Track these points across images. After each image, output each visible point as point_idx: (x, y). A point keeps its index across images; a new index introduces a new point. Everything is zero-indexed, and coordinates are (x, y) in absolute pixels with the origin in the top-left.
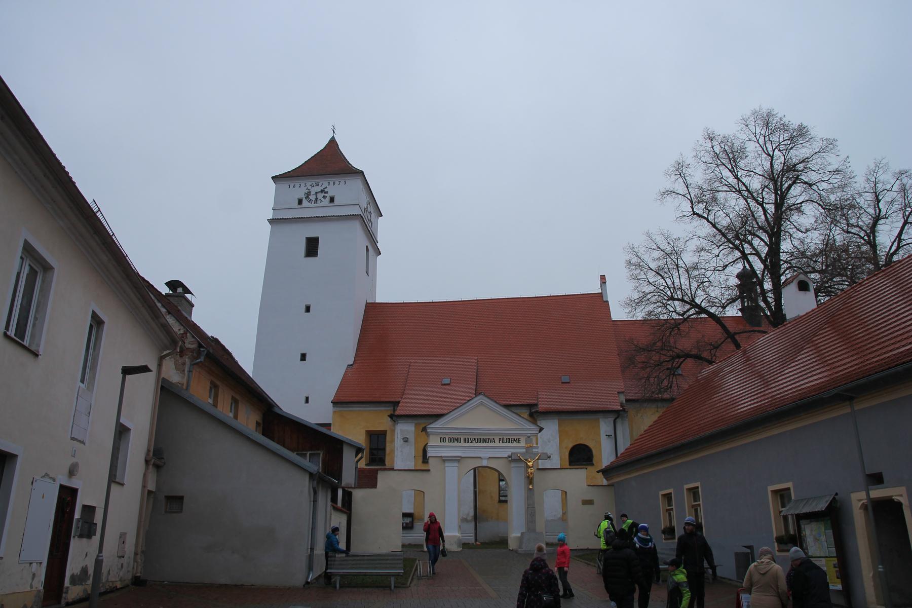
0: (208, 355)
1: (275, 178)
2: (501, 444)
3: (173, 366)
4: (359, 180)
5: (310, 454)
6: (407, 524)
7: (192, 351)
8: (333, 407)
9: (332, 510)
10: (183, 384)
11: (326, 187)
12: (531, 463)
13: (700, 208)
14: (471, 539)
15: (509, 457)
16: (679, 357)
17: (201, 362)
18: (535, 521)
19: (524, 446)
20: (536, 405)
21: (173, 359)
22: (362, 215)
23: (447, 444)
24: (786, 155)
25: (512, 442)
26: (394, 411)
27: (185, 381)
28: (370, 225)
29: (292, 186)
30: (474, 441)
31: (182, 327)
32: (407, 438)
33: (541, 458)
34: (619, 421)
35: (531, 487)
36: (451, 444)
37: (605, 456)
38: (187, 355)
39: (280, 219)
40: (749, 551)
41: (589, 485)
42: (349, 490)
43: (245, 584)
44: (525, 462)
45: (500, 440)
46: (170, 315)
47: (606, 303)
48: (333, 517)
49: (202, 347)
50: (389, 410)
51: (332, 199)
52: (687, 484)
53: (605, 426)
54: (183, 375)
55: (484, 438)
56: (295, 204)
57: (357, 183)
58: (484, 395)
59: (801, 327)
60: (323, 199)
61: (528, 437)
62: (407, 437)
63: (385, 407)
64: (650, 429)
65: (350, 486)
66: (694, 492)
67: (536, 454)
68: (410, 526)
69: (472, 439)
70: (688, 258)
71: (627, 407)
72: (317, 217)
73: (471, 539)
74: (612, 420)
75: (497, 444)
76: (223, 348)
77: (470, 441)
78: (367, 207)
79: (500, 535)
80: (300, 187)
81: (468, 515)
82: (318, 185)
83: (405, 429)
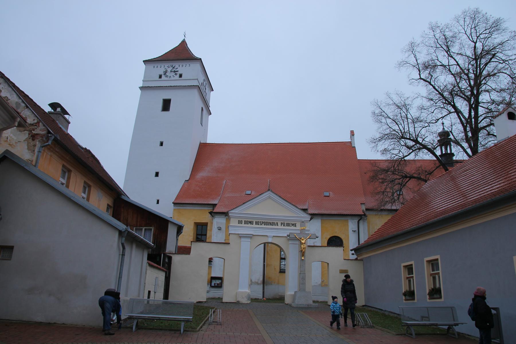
0: (56, 140)
1: (144, 61)
2: (283, 227)
3: (26, 147)
4: (199, 64)
5: (145, 229)
6: (218, 284)
7: (42, 136)
9: (148, 266)
10: (32, 161)
11: (177, 68)
12: (304, 241)
13: (425, 75)
14: (260, 296)
15: (288, 236)
16: (406, 177)
17: (49, 145)
18: (305, 283)
19: (299, 229)
21: (26, 142)
22: (199, 86)
23: (243, 225)
24: (484, 43)
25: (291, 226)
26: (213, 210)
27: (34, 159)
28: (205, 94)
29: (156, 66)
30: (263, 224)
31: (36, 118)
32: (221, 228)
33: (310, 238)
34: (361, 222)
35: (303, 258)
36: (246, 225)
37: (352, 242)
38: (37, 139)
39: (147, 87)
41: (345, 259)
42: (170, 255)
43: (57, 323)
44: (299, 240)
45: (282, 224)
46: (28, 109)
47: (353, 148)
49: (51, 133)
50: (210, 209)
51: (181, 76)
52: (427, 257)
53: (352, 225)
54: (33, 154)
55: (270, 223)
56: (157, 78)
57: (196, 66)
58: (272, 191)
59: (462, 181)
60: (175, 76)
62: (221, 227)
63: (208, 207)
64: (389, 222)
65: (172, 253)
66: (434, 264)
67: (308, 234)
68: (220, 286)
69: (261, 222)
70: (414, 113)
71: (367, 213)
73: (260, 296)
74: (356, 221)
75: (279, 227)
76: (93, 156)
78: (203, 83)
79: (279, 294)
80: (161, 67)
81: (259, 280)
83: (219, 221)
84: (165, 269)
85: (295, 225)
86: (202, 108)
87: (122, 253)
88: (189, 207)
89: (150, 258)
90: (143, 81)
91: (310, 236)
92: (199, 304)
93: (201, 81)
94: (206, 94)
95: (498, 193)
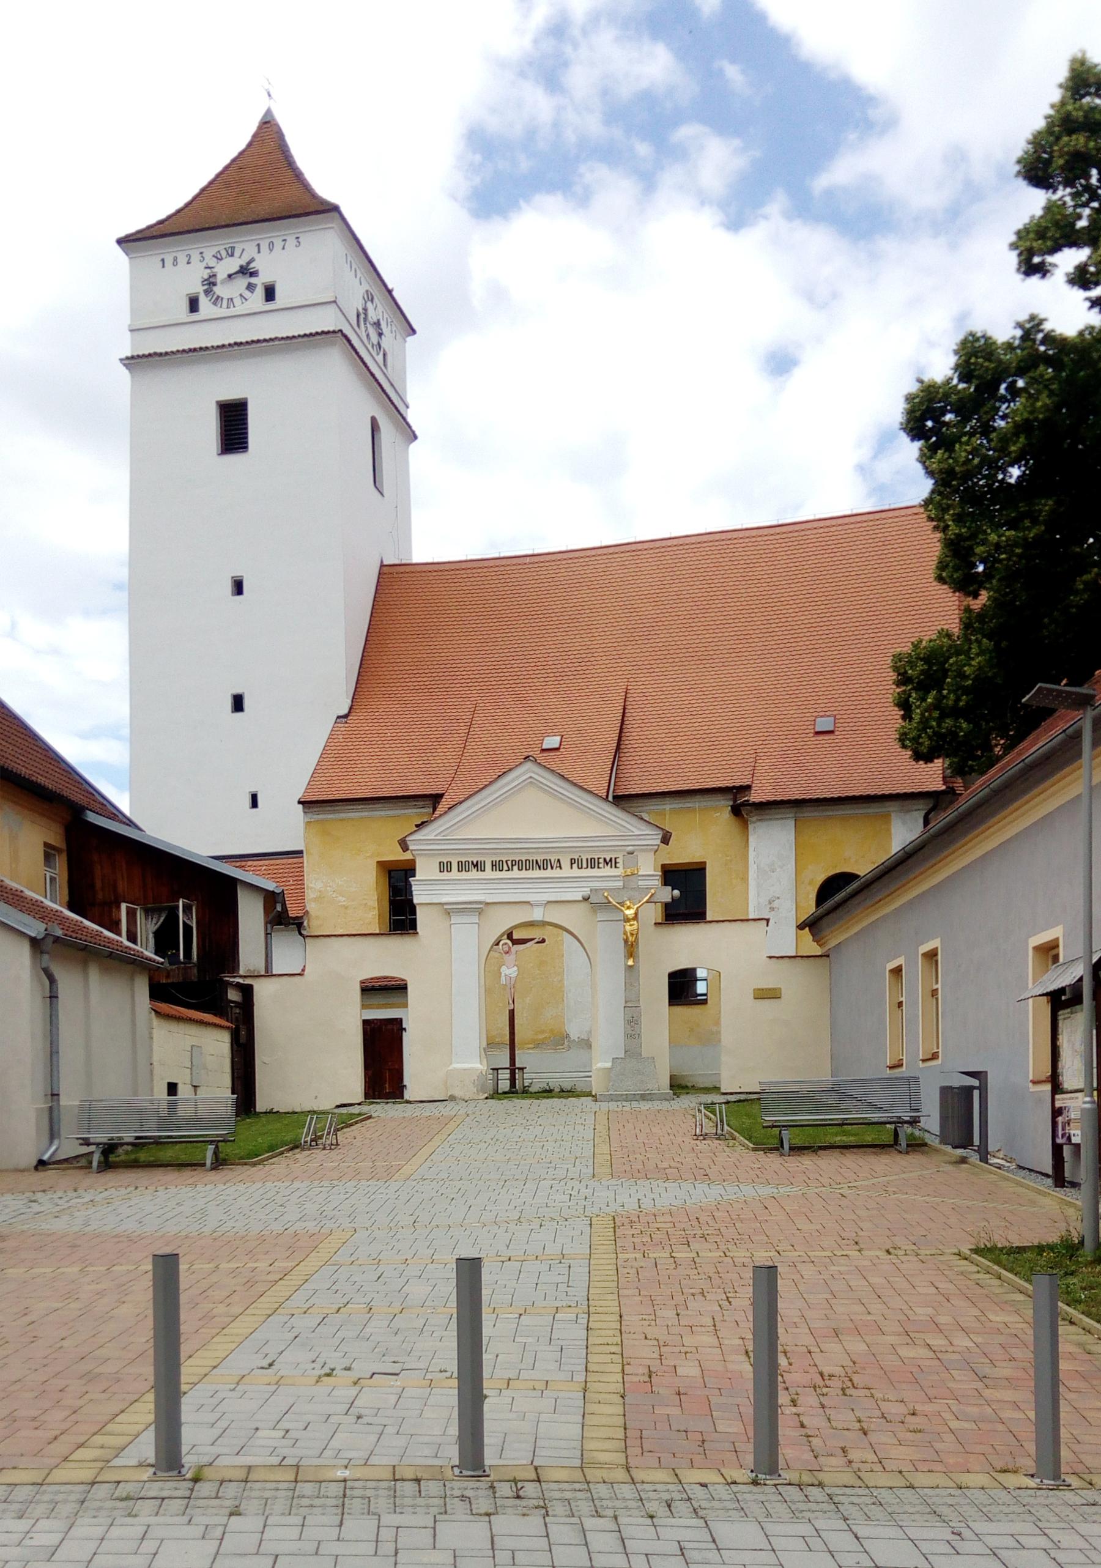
1: (120, 242)
2: (576, 872)
8: (305, 812)
11: (252, 260)
15: (586, 899)
20: (748, 788)
23: (455, 874)
25: (601, 865)
28: (380, 358)
29: (169, 261)
30: (515, 868)
35: (630, 963)
36: (464, 875)
40: (976, 1083)
41: (770, 957)
45: (572, 862)
48: (156, 1033)
51: (270, 293)
60: (247, 294)
61: (629, 853)
69: (509, 863)
72: (236, 344)
75: (566, 871)
77: (505, 867)
78: (365, 310)
82: (232, 255)
84: (227, 1021)
85: (616, 863)
86: (374, 421)
87: (50, 992)
88: (357, 811)
89: (158, 993)
90: (131, 331)
91: (652, 895)
92: (344, 1110)
93: (353, 302)
94: (384, 355)
95: (768, 811)
